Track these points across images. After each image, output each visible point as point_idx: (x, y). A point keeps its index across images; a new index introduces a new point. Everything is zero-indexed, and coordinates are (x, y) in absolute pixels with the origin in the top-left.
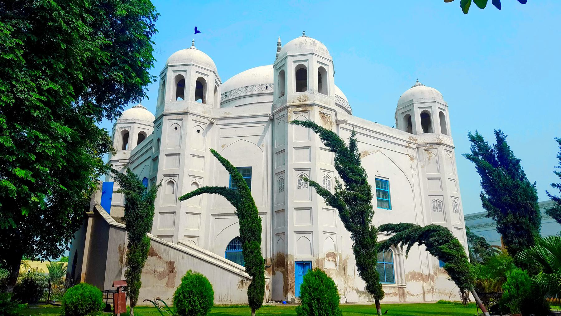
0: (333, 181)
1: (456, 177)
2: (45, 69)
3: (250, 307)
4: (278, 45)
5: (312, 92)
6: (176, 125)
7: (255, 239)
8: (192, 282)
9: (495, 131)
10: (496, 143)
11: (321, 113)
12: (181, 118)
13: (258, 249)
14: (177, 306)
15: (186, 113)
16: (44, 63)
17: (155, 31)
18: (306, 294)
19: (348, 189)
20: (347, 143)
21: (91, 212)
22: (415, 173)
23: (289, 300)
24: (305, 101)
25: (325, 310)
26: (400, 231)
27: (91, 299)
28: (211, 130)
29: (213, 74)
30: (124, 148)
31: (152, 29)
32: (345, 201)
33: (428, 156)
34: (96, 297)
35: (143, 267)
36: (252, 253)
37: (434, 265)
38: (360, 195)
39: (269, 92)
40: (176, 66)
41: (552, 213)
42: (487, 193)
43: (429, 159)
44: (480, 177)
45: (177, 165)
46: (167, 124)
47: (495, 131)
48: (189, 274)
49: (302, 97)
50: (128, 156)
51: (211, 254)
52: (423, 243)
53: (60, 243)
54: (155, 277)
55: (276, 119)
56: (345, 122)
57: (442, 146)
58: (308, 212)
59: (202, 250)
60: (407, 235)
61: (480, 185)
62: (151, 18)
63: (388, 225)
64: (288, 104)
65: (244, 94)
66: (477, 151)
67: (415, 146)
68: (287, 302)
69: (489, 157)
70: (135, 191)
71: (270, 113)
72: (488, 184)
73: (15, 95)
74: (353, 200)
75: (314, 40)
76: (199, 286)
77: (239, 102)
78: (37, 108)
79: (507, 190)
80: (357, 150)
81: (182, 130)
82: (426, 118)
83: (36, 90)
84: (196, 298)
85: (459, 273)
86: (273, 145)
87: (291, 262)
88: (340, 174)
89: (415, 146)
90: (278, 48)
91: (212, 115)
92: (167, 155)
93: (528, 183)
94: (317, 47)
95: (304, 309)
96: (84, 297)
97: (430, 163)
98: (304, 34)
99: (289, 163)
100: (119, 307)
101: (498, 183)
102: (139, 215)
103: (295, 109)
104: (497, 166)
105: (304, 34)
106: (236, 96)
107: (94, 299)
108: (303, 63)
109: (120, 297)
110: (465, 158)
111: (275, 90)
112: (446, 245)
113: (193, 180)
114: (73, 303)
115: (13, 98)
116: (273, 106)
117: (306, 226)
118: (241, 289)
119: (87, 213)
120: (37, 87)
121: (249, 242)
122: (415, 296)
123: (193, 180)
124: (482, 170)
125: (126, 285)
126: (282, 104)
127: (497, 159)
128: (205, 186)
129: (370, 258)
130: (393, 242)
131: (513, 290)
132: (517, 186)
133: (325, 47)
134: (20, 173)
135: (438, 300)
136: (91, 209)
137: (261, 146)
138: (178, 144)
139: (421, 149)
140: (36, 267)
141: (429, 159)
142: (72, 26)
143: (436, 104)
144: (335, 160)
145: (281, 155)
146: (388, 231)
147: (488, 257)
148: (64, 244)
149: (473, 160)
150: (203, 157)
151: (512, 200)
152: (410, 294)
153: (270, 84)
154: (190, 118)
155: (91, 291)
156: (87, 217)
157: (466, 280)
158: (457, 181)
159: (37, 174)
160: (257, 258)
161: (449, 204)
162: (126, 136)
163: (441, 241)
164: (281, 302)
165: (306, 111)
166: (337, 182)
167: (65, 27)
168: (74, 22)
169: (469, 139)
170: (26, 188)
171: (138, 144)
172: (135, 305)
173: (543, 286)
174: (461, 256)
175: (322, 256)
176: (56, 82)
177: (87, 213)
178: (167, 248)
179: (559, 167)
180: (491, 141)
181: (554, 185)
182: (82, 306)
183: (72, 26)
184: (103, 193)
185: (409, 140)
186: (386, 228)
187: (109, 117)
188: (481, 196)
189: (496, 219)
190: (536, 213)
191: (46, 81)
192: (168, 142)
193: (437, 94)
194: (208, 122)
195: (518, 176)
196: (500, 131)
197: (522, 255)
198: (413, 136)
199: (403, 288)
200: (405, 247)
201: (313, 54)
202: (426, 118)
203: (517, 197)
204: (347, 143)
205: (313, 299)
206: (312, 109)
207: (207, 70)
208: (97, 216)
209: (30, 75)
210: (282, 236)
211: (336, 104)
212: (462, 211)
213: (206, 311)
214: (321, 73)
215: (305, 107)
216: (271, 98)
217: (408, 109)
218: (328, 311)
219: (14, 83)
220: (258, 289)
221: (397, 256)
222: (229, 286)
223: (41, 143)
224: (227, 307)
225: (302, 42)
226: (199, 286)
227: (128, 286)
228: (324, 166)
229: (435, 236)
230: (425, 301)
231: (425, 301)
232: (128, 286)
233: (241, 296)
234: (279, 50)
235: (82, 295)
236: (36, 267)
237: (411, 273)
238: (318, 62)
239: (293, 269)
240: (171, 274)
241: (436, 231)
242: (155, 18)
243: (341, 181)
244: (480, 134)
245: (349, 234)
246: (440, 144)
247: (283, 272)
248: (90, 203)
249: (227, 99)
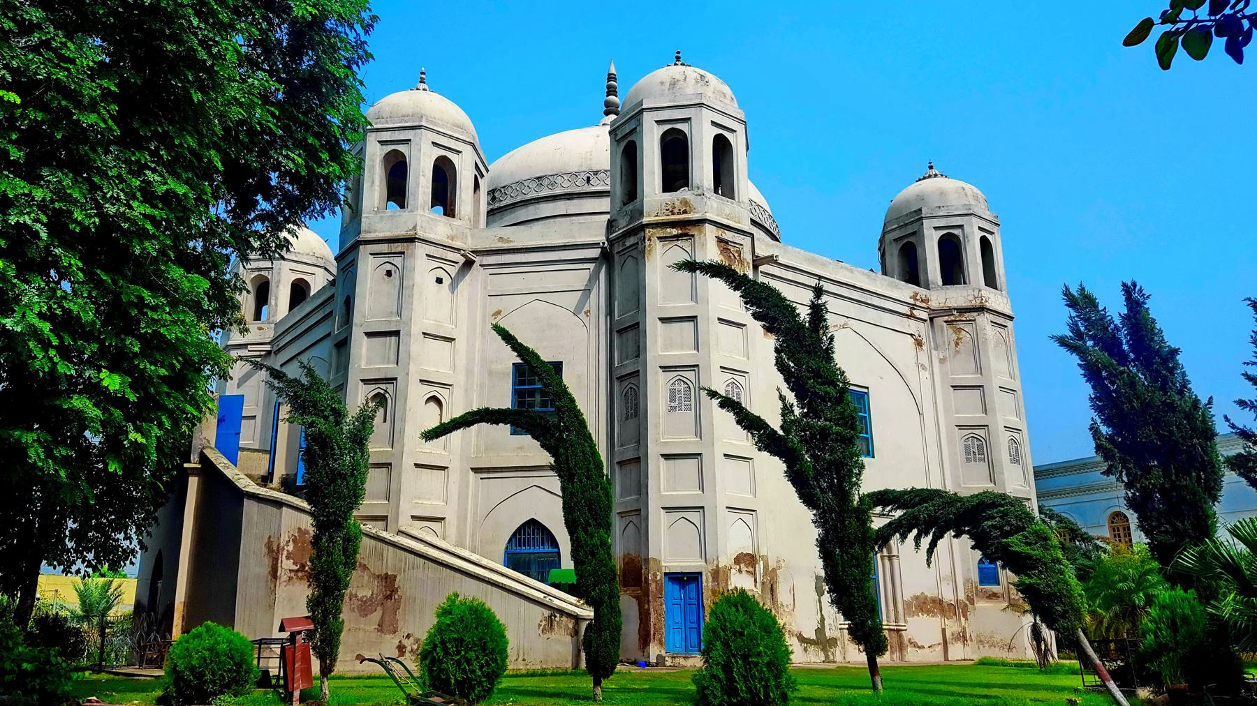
0: (768, 395)
1: (1016, 385)
2: (157, 148)
3: (590, 673)
4: (609, 80)
5: (700, 192)
6: (389, 267)
7: (599, 525)
8: (461, 620)
9: (1124, 285)
10: (1125, 311)
11: (720, 240)
12: (399, 249)
13: (605, 546)
14: (430, 671)
15: (411, 240)
16: (156, 136)
17: (369, 56)
18: (718, 644)
19: (804, 415)
20: (804, 313)
21: (194, 463)
22: (925, 374)
23: (653, 660)
24: (685, 212)
25: (761, 679)
26: (913, 506)
27: (232, 658)
28: (467, 277)
29: (470, 148)
30: (258, 316)
31: (360, 52)
32: (801, 442)
33: (954, 337)
34: (243, 655)
35: (346, 587)
36: (593, 554)
37: (967, 581)
38: (836, 429)
39: (593, 189)
40: (387, 129)
41: (1240, 464)
42: (1105, 422)
43: (957, 344)
44: (1089, 386)
45: (393, 357)
46: (368, 267)
47: (1124, 285)
48: (454, 602)
49: (677, 203)
50: (269, 335)
51: (474, 557)
52: (964, 532)
53: (126, 534)
54: (353, 610)
55: (620, 254)
56: (771, 260)
57: (987, 315)
58: (693, 463)
59: (453, 549)
60: (929, 515)
61: (1088, 403)
62: (358, 27)
63: (886, 492)
64: (645, 220)
65: (535, 195)
66: (1082, 329)
67: (924, 315)
68: (648, 664)
69: (1109, 343)
70: (326, 418)
71: (603, 239)
72: (1108, 403)
73: (99, 207)
74: (820, 436)
75: (703, 72)
76: (476, 628)
77: (523, 214)
78: (143, 235)
79: (1150, 415)
80: (827, 328)
81: (402, 278)
82: (951, 249)
83: (138, 194)
84: (472, 654)
85: (1051, 597)
86: (610, 312)
87: (655, 576)
88: (787, 380)
89: (924, 315)
90: (609, 87)
91: (470, 244)
92: (370, 335)
93: (1196, 402)
94: (711, 88)
95: (713, 676)
96: (218, 655)
97: (957, 352)
98: (678, 58)
99: (650, 355)
100: (298, 675)
101: (1130, 401)
102: (331, 472)
103: (660, 232)
104: (1126, 363)
105: (678, 58)
106: (519, 199)
107: (237, 659)
108: (679, 126)
109: (298, 654)
110: (1056, 344)
111: (613, 184)
112: (1019, 536)
113: (429, 391)
114: (192, 669)
115: (96, 215)
116: (611, 225)
117: (687, 494)
118: (548, 635)
119: (186, 465)
120: (141, 189)
121: (586, 531)
122: (927, 650)
123: (429, 391)
124: (1092, 372)
125: (312, 627)
126: (632, 220)
127: (1126, 347)
128: (482, 406)
129: (857, 566)
130: (900, 528)
131: (1165, 633)
132: (1171, 407)
133: (727, 90)
134: (112, 382)
135: (976, 657)
136: (195, 457)
137: (582, 315)
138: (395, 310)
139: (939, 321)
140: (58, 590)
141: (957, 344)
142: (215, 50)
143: (974, 219)
144: (777, 350)
145: (631, 334)
146: (885, 505)
147: (1087, 562)
148: (134, 537)
149: (1073, 349)
150: (451, 340)
151: (1161, 437)
152: (915, 645)
153: (596, 173)
154: (420, 250)
155: (230, 642)
156: (185, 474)
157: (1066, 612)
158: (1020, 393)
159: (139, 381)
160: (605, 566)
161: (1002, 442)
162: (263, 293)
163: (1007, 528)
164: (635, 663)
165: (686, 235)
166: (782, 398)
167: (202, 55)
168: (217, 42)
169: (1064, 302)
170: (118, 413)
171: (291, 308)
172: (331, 671)
173: (1236, 622)
174: (1053, 561)
175: (725, 560)
176: (177, 177)
177: (186, 465)
178: (379, 544)
179: (1254, 363)
180: (1114, 307)
181: (1242, 403)
182: (213, 675)
183: (215, 50)
184: (219, 421)
185: (912, 301)
186: (884, 498)
187: (265, 252)
188: (1091, 429)
189: (1125, 479)
190: (1213, 467)
191: (160, 175)
192: (371, 303)
193: (976, 197)
194: (462, 260)
195: (1174, 384)
196: (1134, 285)
197: (1188, 558)
198: (922, 292)
199: (898, 631)
200: (926, 541)
201: (700, 105)
202: (951, 249)
203: (1171, 432)
204: (804, 313)
205: (734, 656)
206: (700, 232)
207: (457, 139)
208: (209, 471)
209: (128, 162)
210: (634, 519)
211: (753, 222)
212: (1029, 461)
213: (492, 684)
214: (722, 147)
215: (685, 228)
216: (604, 204)
217: (910, 230)
218: (767, 680)
219: (96, 180)
220: (607, 633)
221: (886, 561)
222: (535, 630)
223: (150, 314)
224: (522, 676)
225: (677, 77)
226: (476, 628)
227: (316, 629)
228: (751, 363)
229: (994, 518)
230: (946, 659)
231: (946, 659)
232: (316, 629)
233: (558, 649)
234: (611, 91)
235: (210, 650)
236: (58, 590)
237: (916, 598)
238: (714, 123)
239: (660, 590)
240: (389, 603)
241: (997, 507)
242: (368, 28)
243: (791, 397)
244: (1088, 290)
245: (810, 514)
246: (981, 309)
247: (637, 598)
248: (190, 443)
249: (497, 205)
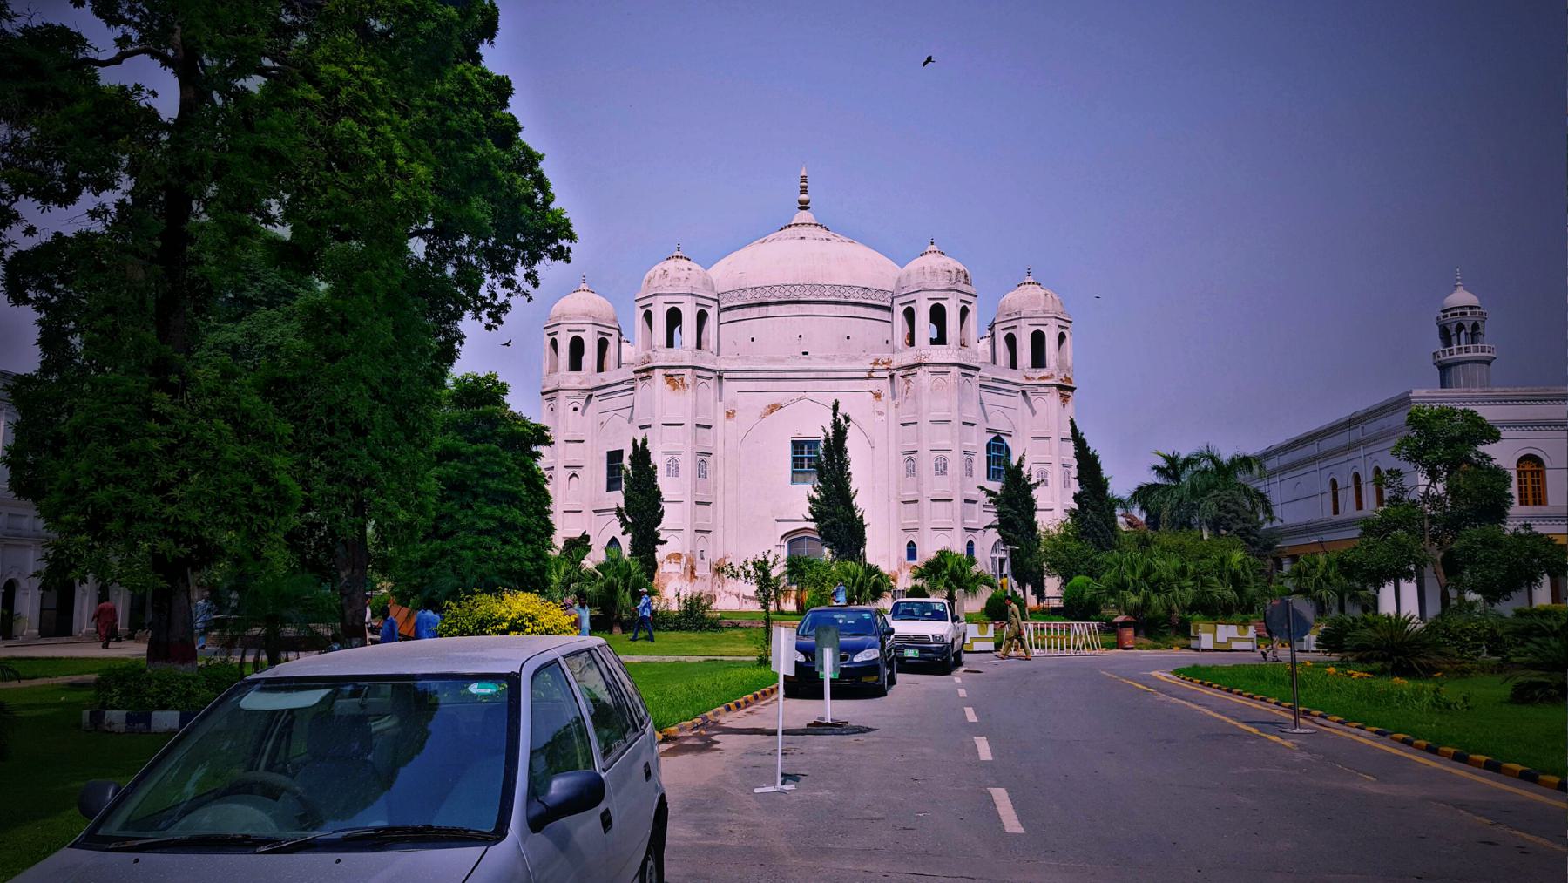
123: (570, 471)
154: (562, 395)
234: (804, 191)
246: (919, 365)
